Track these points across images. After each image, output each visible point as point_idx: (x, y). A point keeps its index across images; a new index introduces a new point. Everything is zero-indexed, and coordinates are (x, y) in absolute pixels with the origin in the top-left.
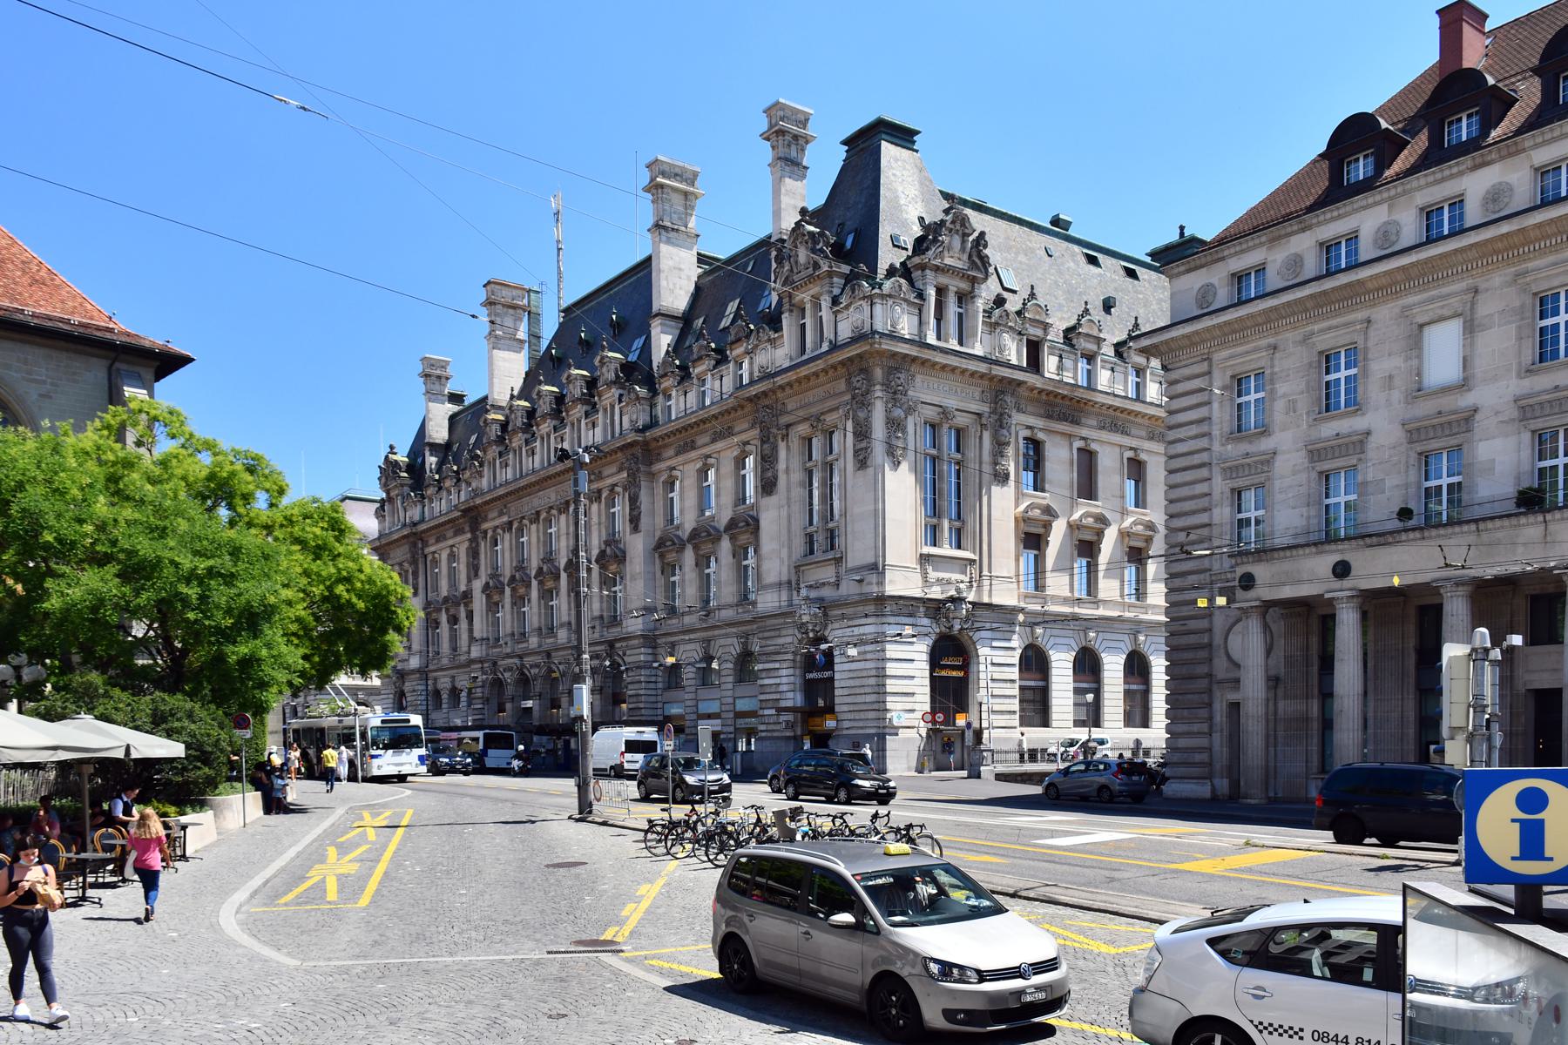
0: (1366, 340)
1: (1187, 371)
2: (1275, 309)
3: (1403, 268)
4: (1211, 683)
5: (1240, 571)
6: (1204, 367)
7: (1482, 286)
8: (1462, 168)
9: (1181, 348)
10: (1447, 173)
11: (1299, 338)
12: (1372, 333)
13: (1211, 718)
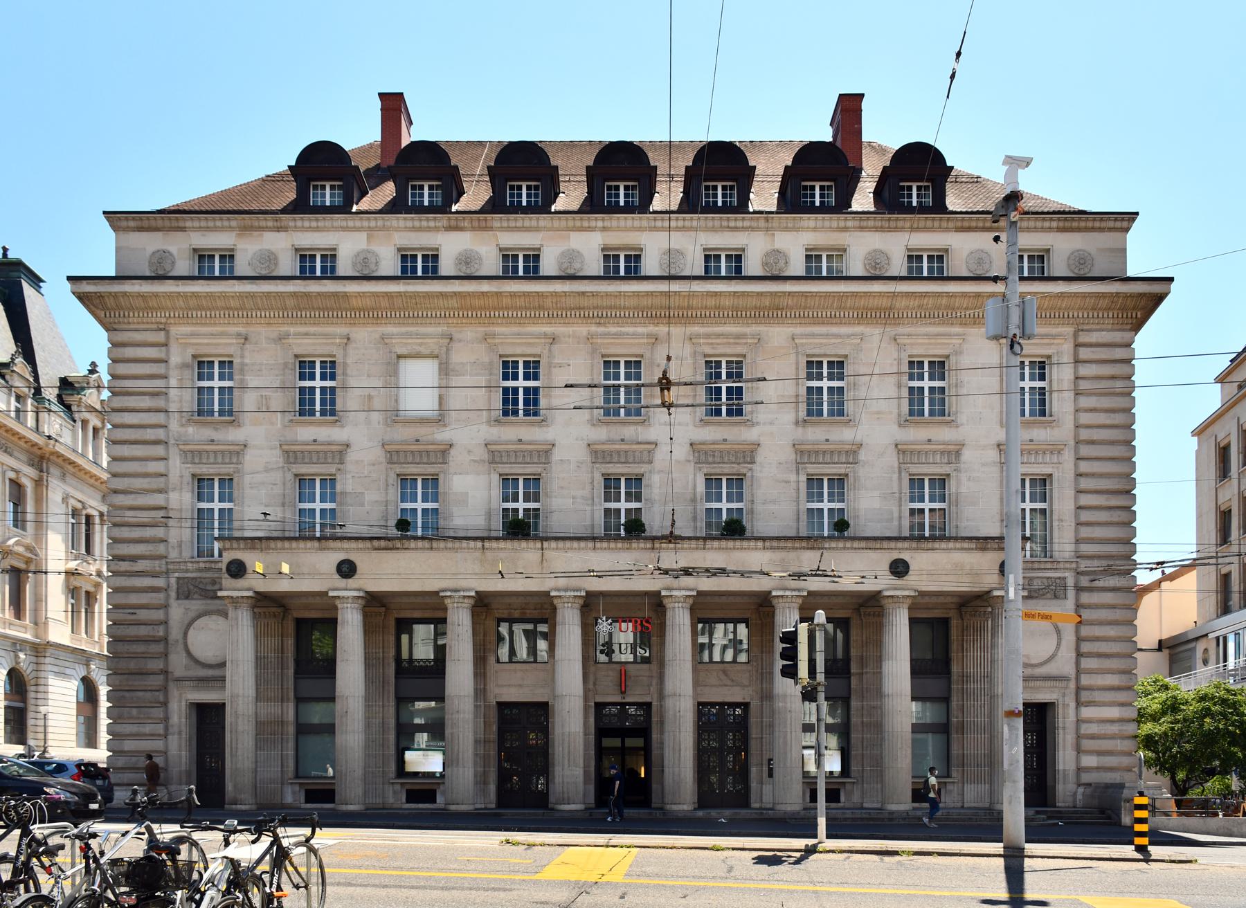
0: (345, 356)
1: (138, 337)
2: (252, 296)
3: (388, 295)
4: (167, 680)
5: (228, 557)
6: (160, 337)
7: (456, 336)
8: (439, 224)
9: (131, 308)
10: (424, 224)
11: (275, 335)
12: (351, 351)
13: (166, 719)
